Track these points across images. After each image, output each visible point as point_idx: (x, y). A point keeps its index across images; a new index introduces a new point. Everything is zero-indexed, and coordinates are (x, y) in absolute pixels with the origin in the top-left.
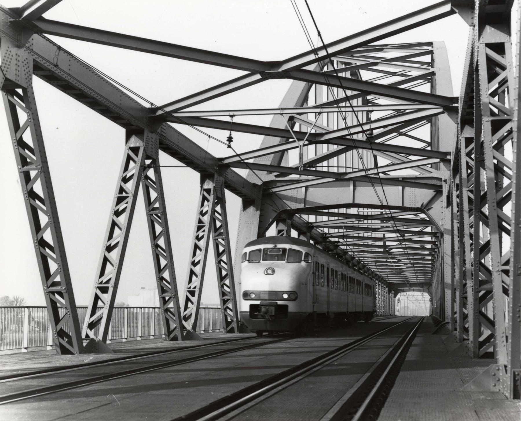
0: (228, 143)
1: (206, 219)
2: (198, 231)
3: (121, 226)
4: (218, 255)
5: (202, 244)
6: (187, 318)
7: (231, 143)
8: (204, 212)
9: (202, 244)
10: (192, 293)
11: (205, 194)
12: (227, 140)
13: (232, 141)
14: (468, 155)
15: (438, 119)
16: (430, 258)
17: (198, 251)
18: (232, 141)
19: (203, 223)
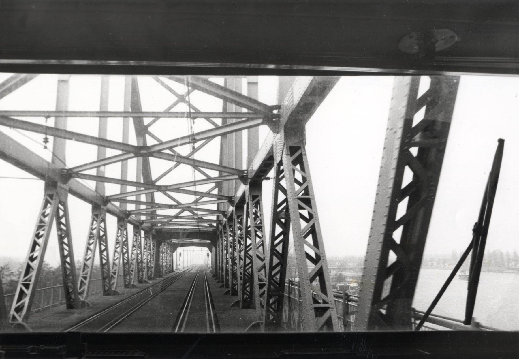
0: (44, 144)
1: (95, 232)
2: (89, 240)
3: (40, 244)
4: (101, 252)
5: (92, 247)
6: (81, 293)
7: (47, 144)
8: (46, 214)
9: (92, 247)
10: (85, 278)
11: (95, 217)
12: (44, 142)
13: (48, 142)
14: (261, 295)
15: (257, 131)
16: (270, 309)
17: (89, 251)
18: (48, 142)
19: (44, 223)
